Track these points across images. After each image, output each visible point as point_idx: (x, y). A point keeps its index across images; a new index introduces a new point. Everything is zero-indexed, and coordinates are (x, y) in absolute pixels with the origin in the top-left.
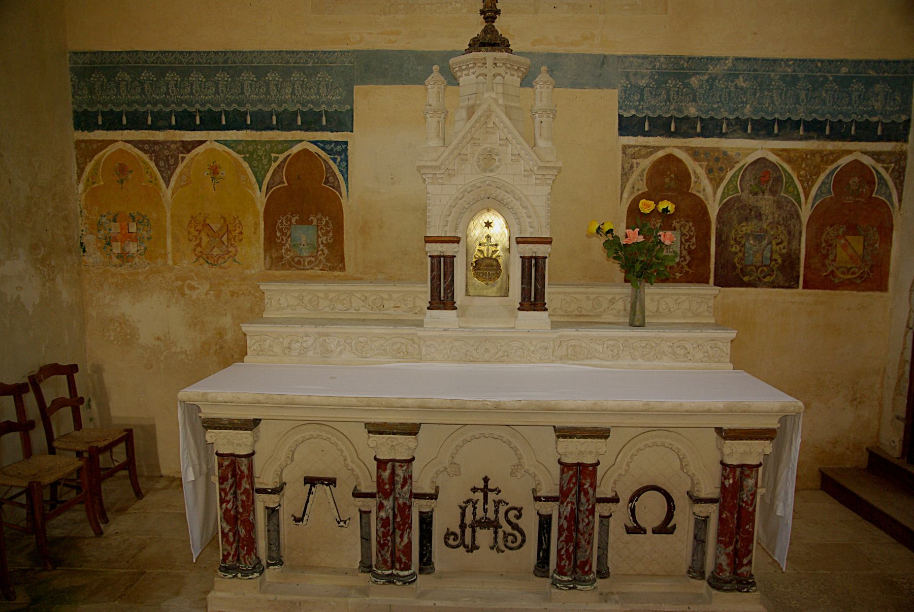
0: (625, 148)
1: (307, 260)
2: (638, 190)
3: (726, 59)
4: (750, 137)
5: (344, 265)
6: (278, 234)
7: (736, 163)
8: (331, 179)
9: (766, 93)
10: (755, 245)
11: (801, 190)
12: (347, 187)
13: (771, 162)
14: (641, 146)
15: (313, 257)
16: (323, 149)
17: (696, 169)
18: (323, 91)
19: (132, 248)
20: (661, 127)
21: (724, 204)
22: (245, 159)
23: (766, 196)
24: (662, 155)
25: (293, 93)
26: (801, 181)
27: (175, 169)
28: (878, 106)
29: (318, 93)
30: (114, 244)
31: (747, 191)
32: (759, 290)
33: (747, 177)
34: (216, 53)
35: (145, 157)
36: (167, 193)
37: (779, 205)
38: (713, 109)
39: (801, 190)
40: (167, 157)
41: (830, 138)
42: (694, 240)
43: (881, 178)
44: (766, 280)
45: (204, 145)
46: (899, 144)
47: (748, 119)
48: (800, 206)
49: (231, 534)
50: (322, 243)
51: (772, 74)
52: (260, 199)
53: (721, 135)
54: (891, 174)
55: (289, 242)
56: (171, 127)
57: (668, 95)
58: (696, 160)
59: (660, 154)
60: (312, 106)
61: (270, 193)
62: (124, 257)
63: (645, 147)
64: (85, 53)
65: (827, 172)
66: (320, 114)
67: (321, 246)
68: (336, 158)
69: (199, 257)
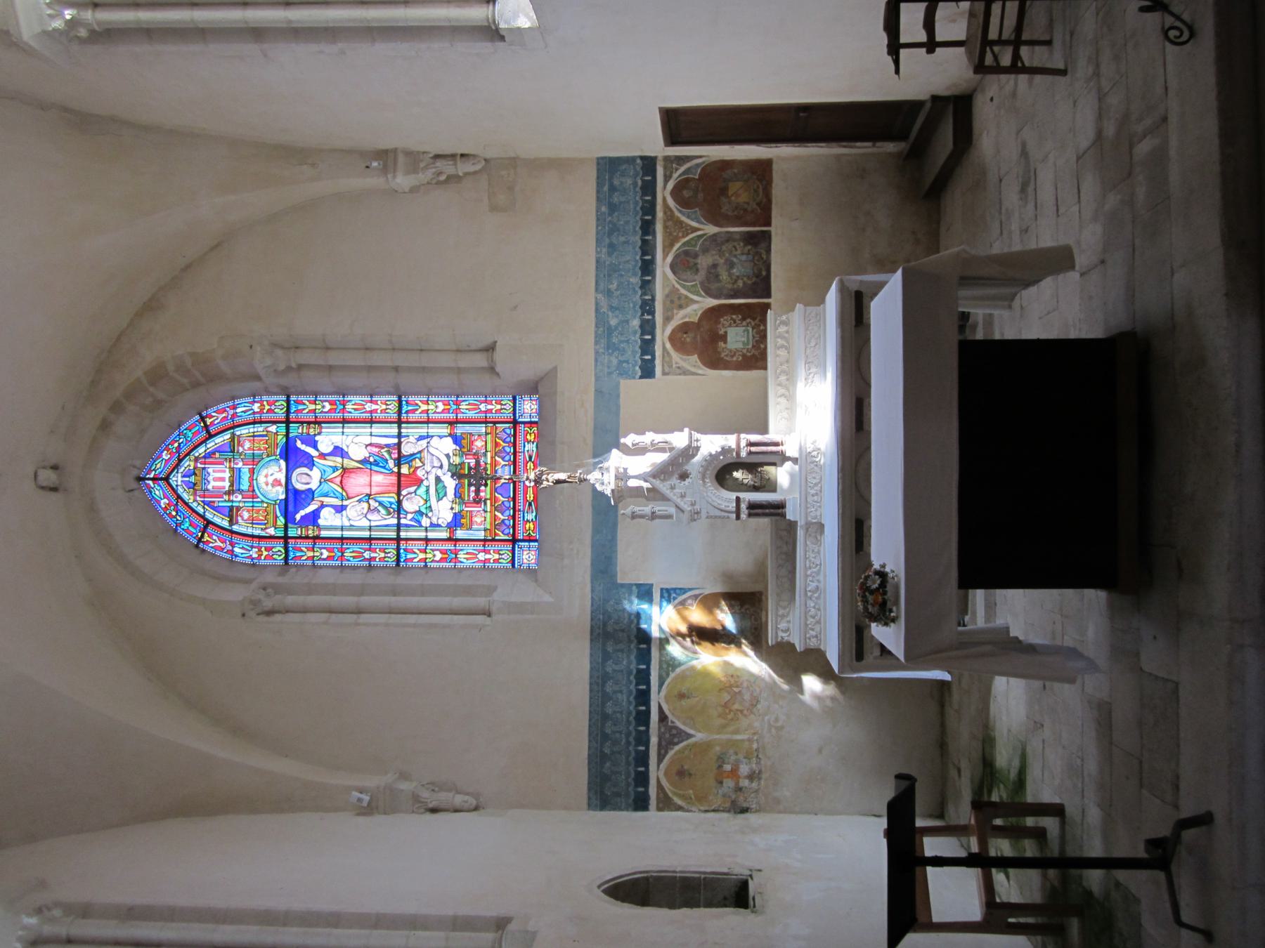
0: (664, 373)
17: (680, 317)
20: (647, 347)
37: (705, 250)
53: (653, 299)
59: (668, 346)
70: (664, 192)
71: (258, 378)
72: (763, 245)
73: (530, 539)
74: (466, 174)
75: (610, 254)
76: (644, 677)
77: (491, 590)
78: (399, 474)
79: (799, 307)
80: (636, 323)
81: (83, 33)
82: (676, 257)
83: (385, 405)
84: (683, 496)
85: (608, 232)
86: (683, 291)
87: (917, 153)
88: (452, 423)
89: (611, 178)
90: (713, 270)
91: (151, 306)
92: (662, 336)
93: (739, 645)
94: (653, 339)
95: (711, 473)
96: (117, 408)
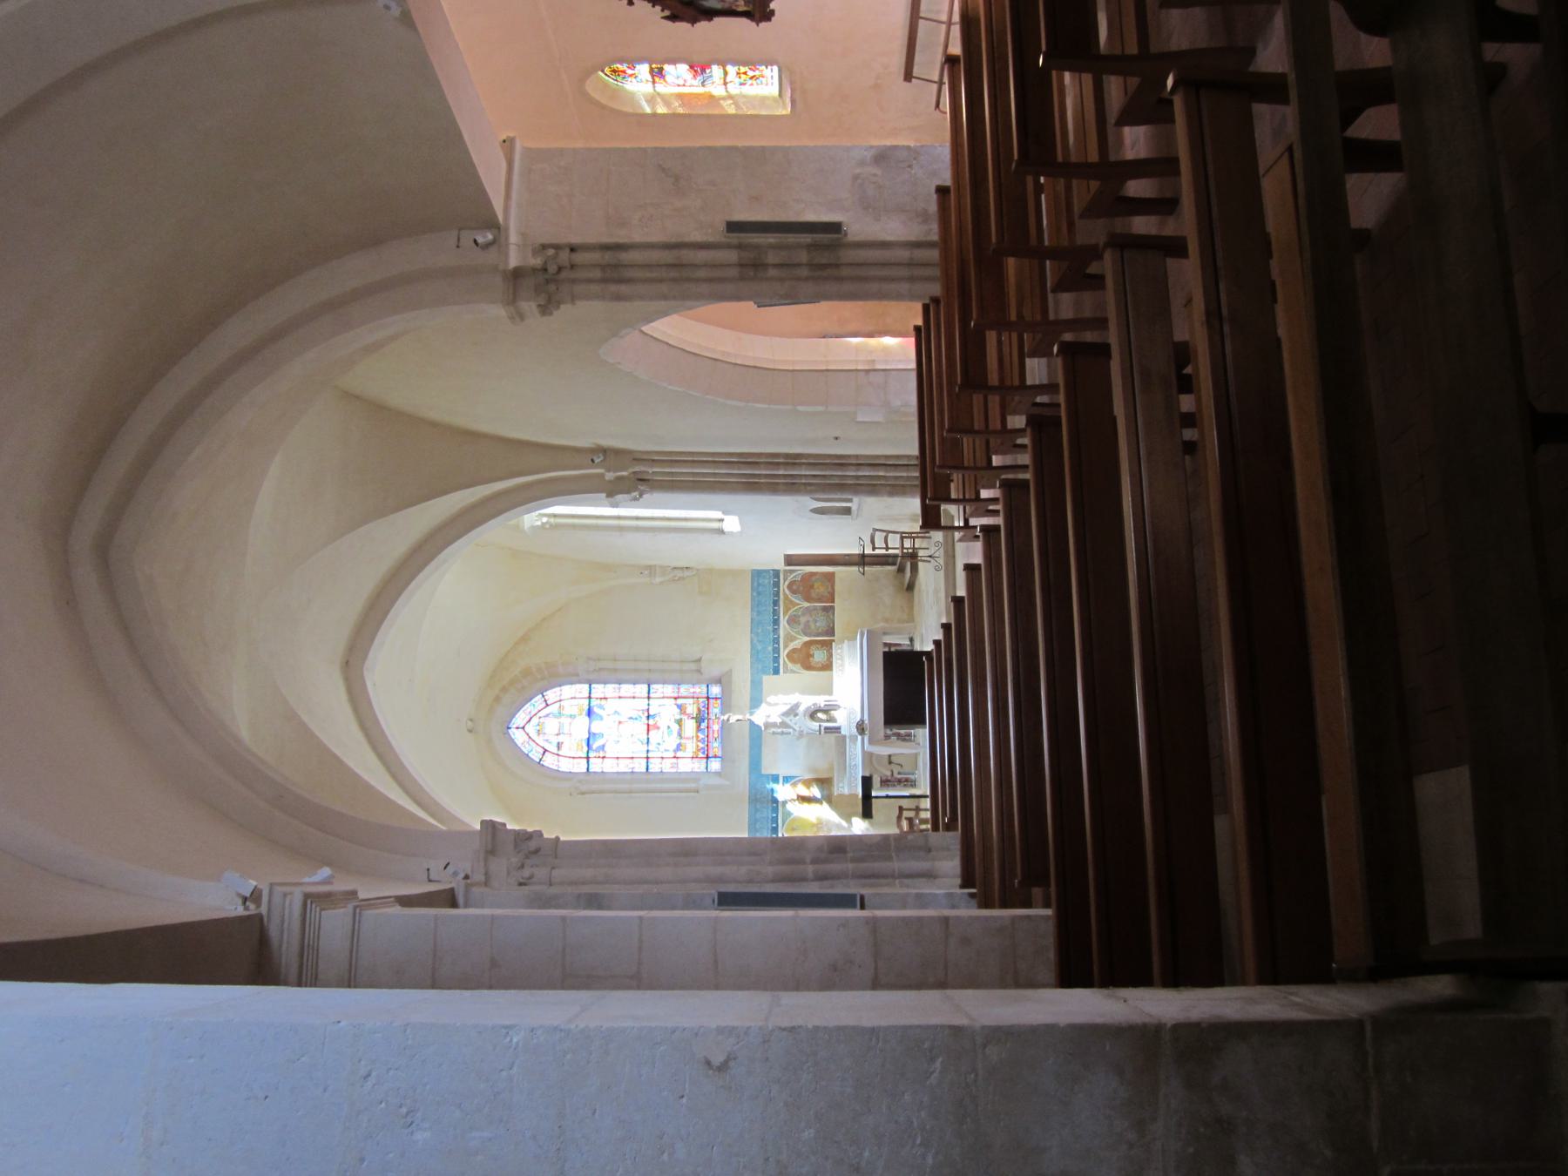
0: (784, 672)
17: (792, 645)
20: (776, 660)
37: (803, 614)
53: (779, 637)
59: (786, 659)
70: (783, 586)
71: (577, 675)
72: (830, 613)
73: (716, 757)
74: (688, 576)
75: (758, 615)
76: (775, 820)
77: (699, 780)
78: (648, 725)
79: (846, 641)
80: (770, 648)
81: (547, 526)
82: (789, 617)
83: (641, 689)
84: (796, 724)
85: (756, 605)
86: (793, 633)
87: (901, 570)
88: (676, 698)
89: (758, 580)
90: (807, 624)
91: (524, 639)
92: (783, 654)
93: (821, 803)
94: (779, 656)
95: (808, 715)
96: (504, 689)
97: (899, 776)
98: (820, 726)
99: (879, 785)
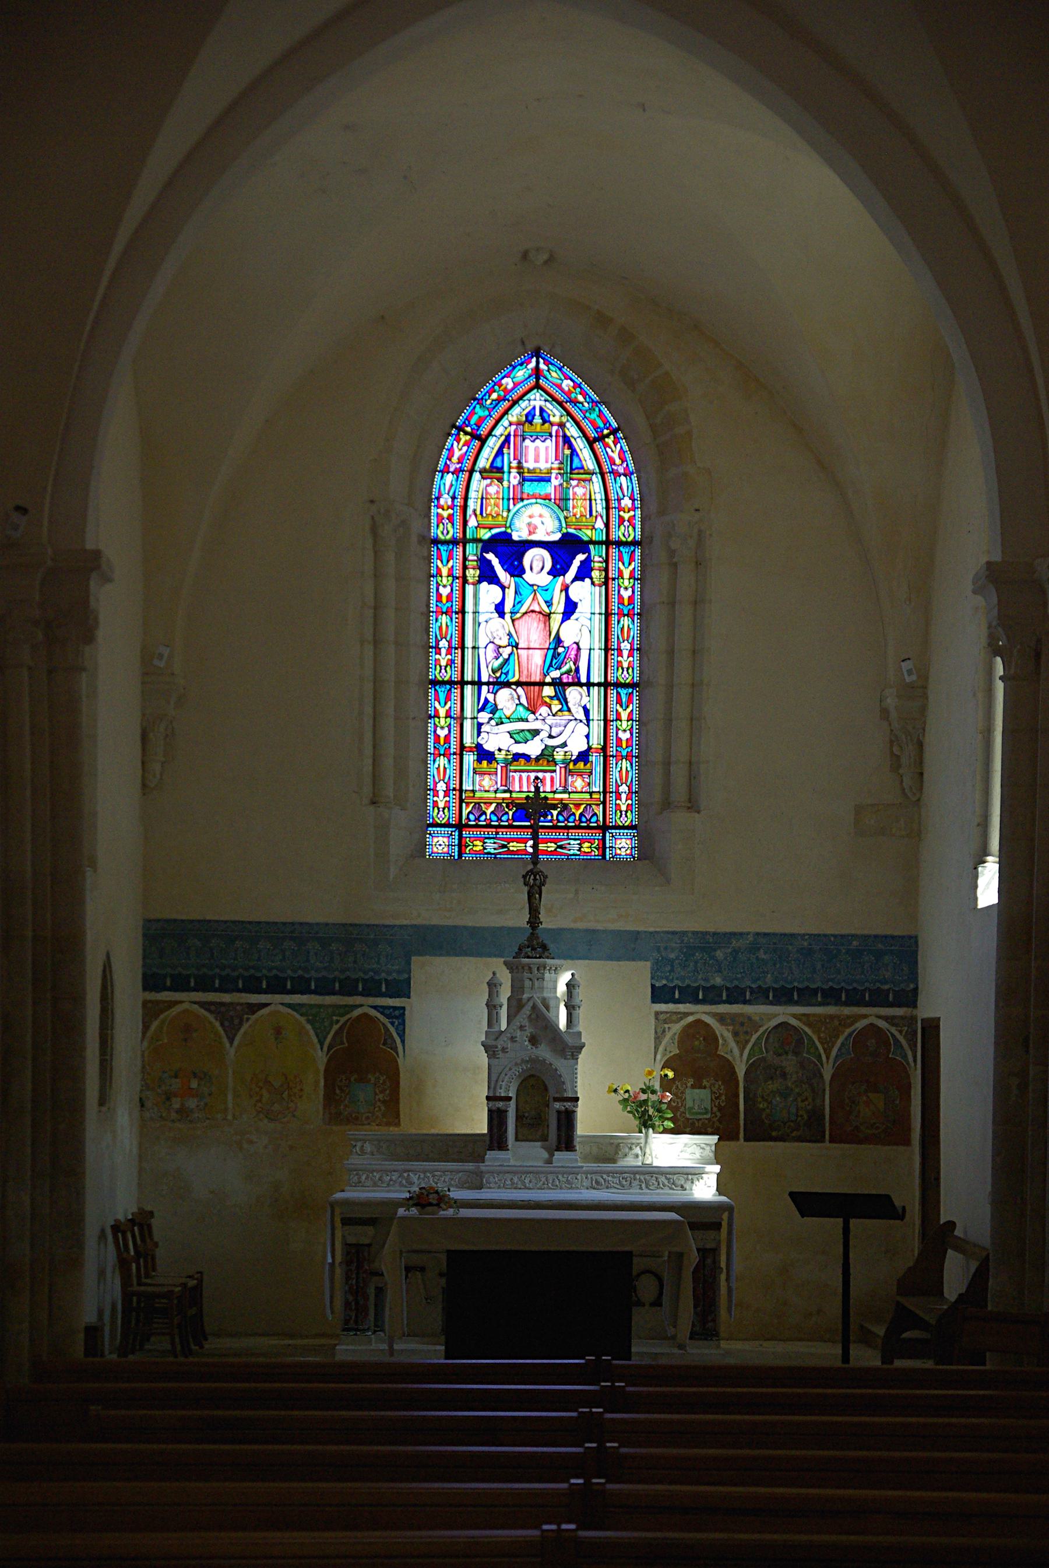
0: (657, 1014)
1: (364, 1116)
2: (670, 1052)
3: (748, 934)
4: (772, 1003)
5: (399, 1121)
6: (338, 1091)
7: (760, 1027)
8: (389, 1041)
9: (785, 964)
10: (781, 1102)
11: (822, 1051)
12: (404, 1048)
13: (793, 1026)
14: (671, 1012)
15: (370, 1113)
16: (382, 1013)
17: (723, 1032)
18: (383, 960)
19: (192, 1103)
20: (689, 995)
21: (751, 1064)
22: (308, 1021)
23: (790, 1057)
24: (691, 1020)
25: (355, 962)
26: (822, 1044)
27: (240, 1028)
28: (888, 975)
29: (378, 963)
30: (174, 1100)
31: (772, 1052)
32: (787, 1144)
33: (771, 1040)
34: (284, 924)
35: (211, 1018)
36: (231, 1052)
37: (802, 1065)
38: (737, 979)
39: (822, 1051)
40: (232, 1017)
41: (847, 1004)
42: (723, 1098)
43: (810, 1039)
44: (794, 1134)
45: (269, 1007)
46: (910, 1010)
47: (769, 988)
48: (822, 1065)
49: (353, 1303)
50: (379, 1100)
51: (790, 948)
52: (321, 1058)
53: (745, 1002)
54: (905, 1037)
55: (348, 1099)
56: (239, 991)
57: (696, 966)
58: (722, 1024)
59: (690, 1019)
60: (373, 974)
61: (331, 1053)
62: (184, 1113)
63: (675, 1013)
64: (158, 920)
65: (846, 1034)
66: (379, 982)
67: (378, 1104)
68: (394, 1022)
69: (260, 1112)
70: (872, 1016)
71: (662, 512)
73: (461, 846)
80: (718, 981)
92: (702, 1012)
97: (371, 1291)
98: (509, 1099)
99: (351, 1240)
